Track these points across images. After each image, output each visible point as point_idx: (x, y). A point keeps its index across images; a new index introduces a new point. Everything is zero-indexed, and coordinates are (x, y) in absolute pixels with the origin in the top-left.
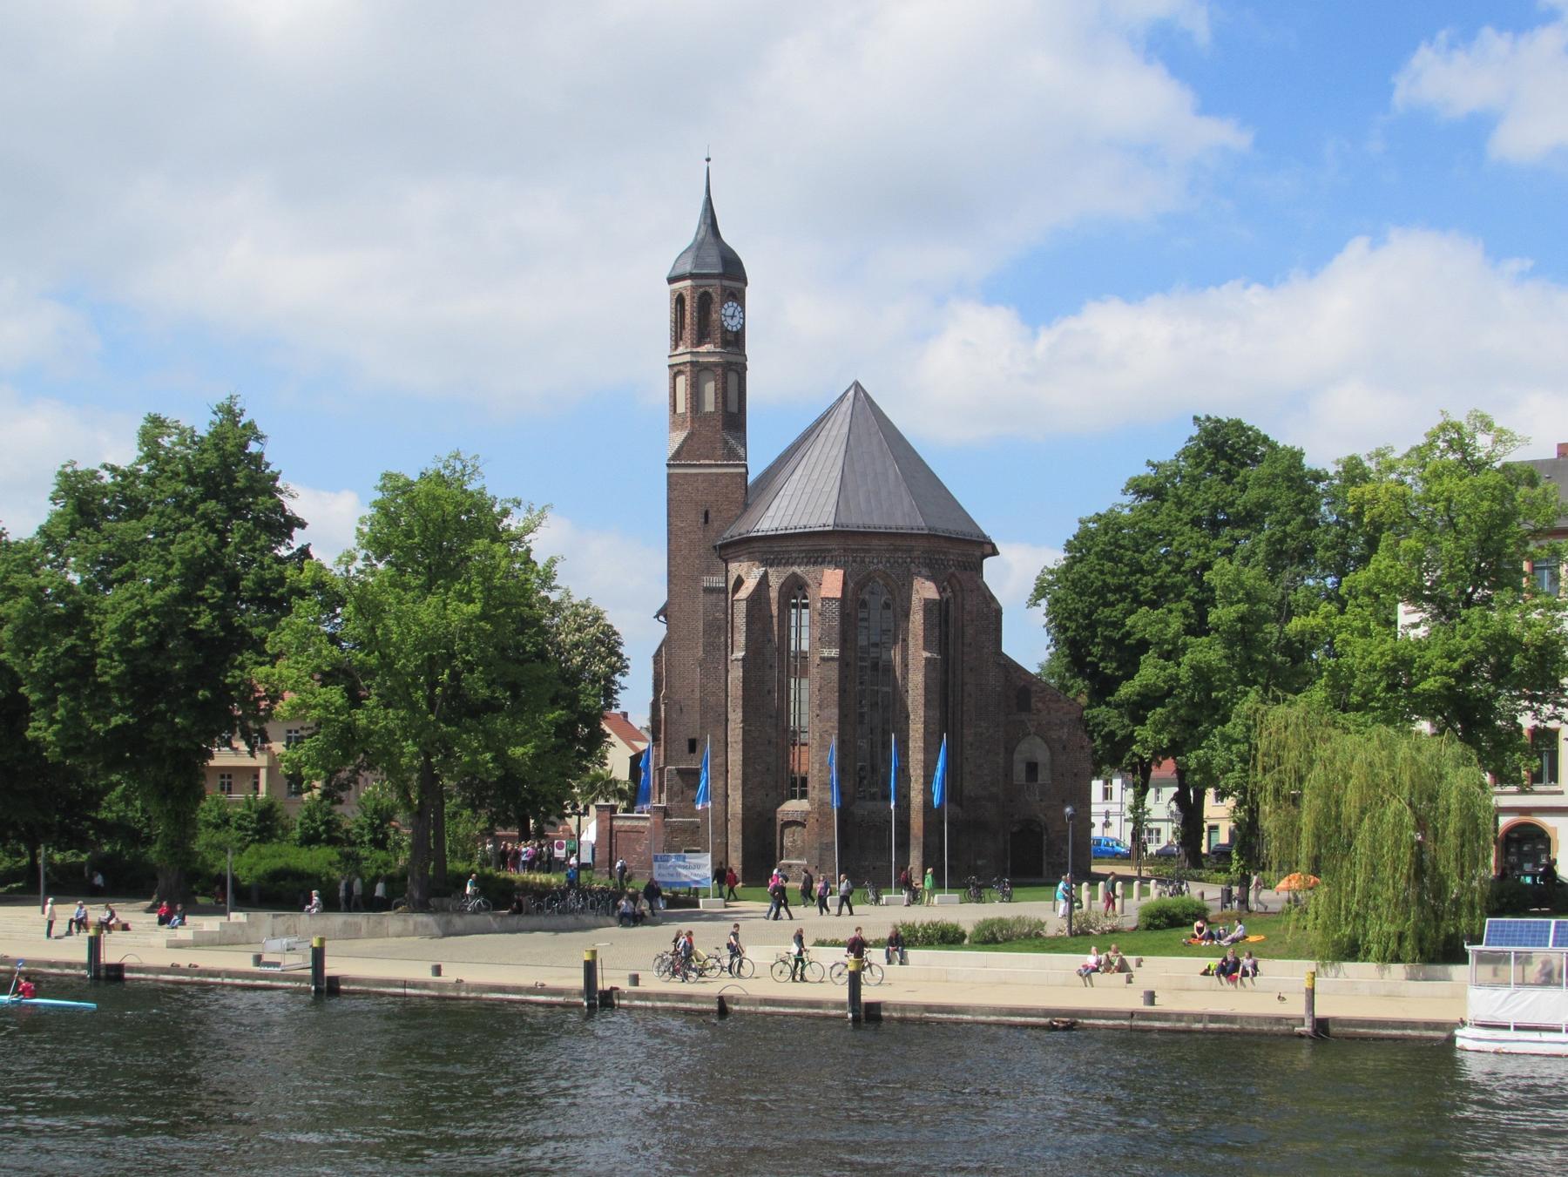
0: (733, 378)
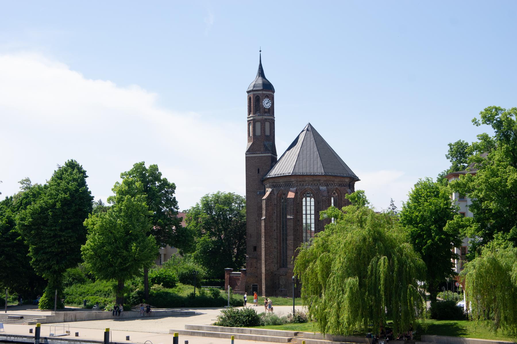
0: (267, 124)
